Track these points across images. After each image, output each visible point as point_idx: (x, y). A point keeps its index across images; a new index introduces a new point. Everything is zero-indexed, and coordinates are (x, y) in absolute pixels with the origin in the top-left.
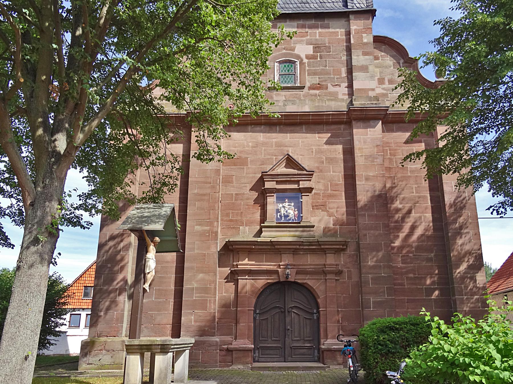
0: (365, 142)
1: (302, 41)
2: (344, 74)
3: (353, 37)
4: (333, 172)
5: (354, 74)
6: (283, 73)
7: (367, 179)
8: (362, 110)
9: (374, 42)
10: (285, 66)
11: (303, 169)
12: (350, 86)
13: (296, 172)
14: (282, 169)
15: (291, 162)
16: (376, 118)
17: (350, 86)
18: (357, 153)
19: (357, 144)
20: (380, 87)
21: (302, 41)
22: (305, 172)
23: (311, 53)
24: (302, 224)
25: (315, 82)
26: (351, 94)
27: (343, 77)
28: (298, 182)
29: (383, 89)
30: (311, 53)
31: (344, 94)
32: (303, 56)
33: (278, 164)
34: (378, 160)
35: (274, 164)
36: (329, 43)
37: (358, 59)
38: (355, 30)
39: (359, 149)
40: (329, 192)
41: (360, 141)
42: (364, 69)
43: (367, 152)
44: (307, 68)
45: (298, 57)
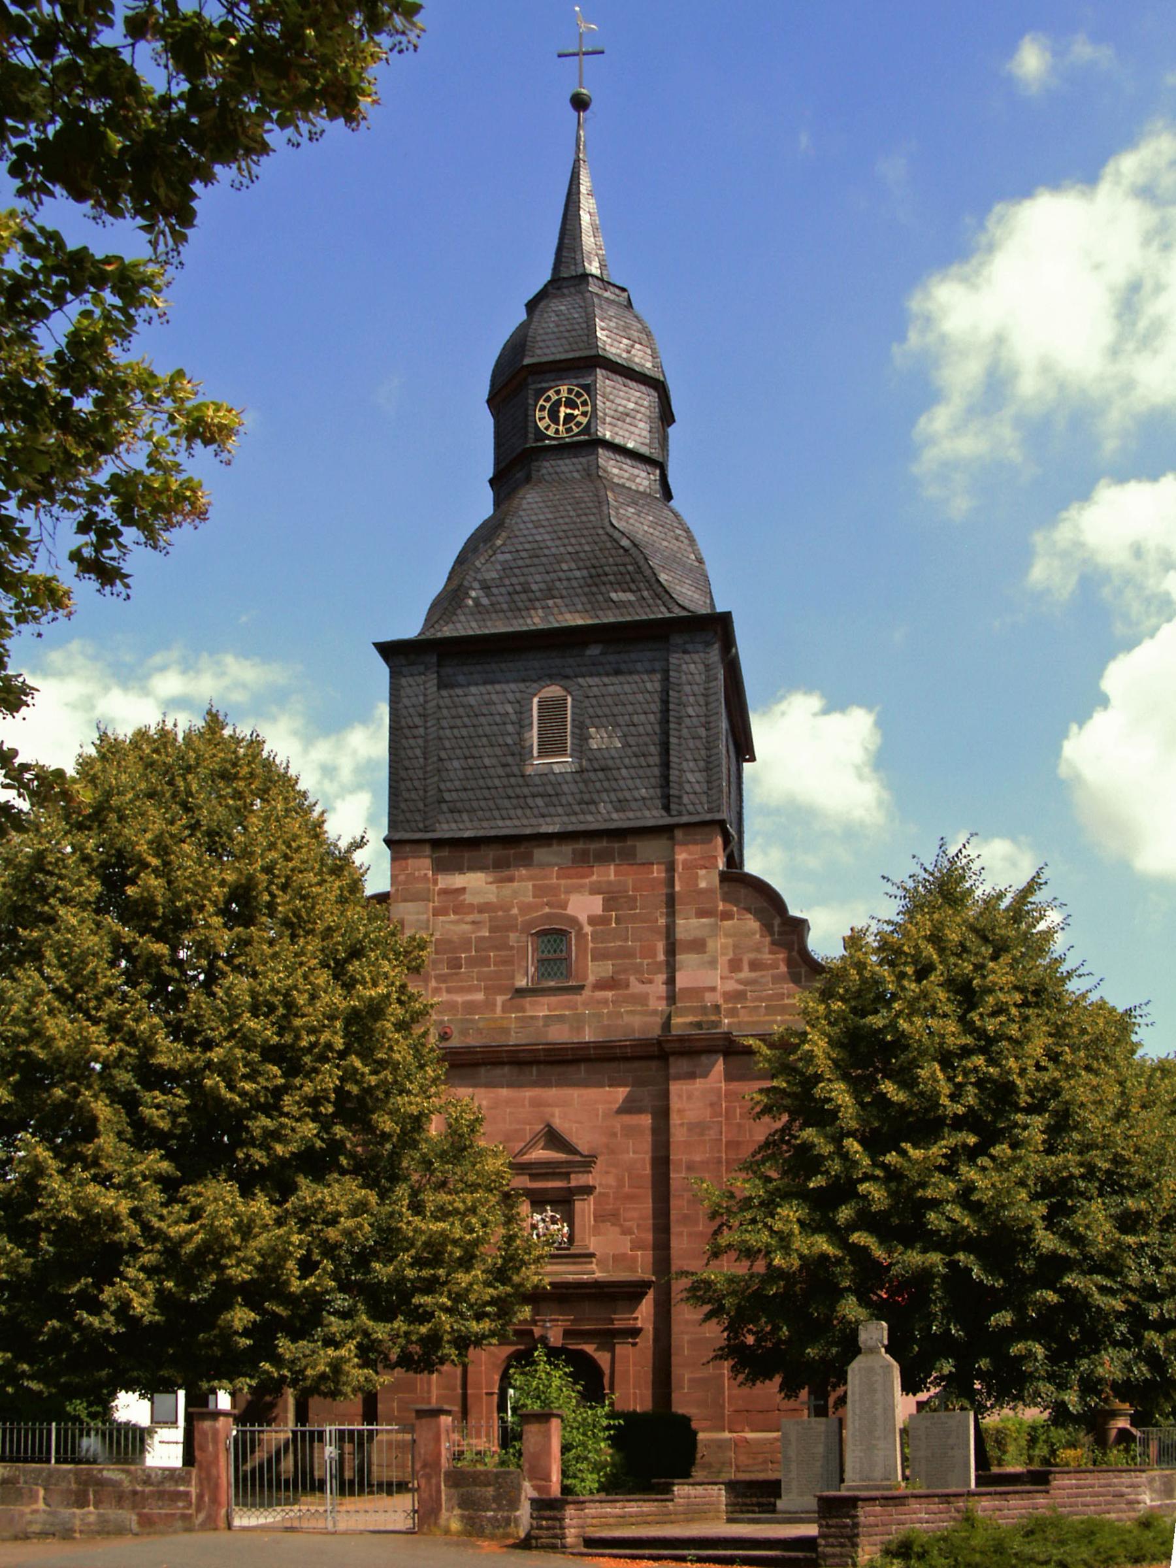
0: (690, 1097)
1: (582, 886)
2: (661, 957)
3: (680, 878)
4: (634, 1152)
5: (678, 957)
6: (545, 955)
7: (690, 1167)
8: (681, 1039)
9: (721, 881)
10: (549, 941)
11: (574, 1152)
12: (671, 981)
13: (561, 1156)
14: (540, 1154)
15: (553, 1138)
16: (711, 1051)
17: (671, 981)
18: (675, 1120)
19: (675, 1104)
20: (732, 978)
21: (582, 886)
22: (578, 1158)
23: (598, 910)
24: (572, 1251)
25: (603, 974)
26: (671, 998)
27: (660, 962)
28: (567, 1176)
29: (739, 982)
30: (598, 910)
31: (659, 998)
32: (583, 918)
33: (530, 1146)
34: (712, 1132)
35: (528, 1139)
36: (634, 889)
37: (688, 926)
38: (685, 862)
39: (679, 1111)
40: (626, 1189)
41: (680, 1096)
42: (698, 946)
43: (692, 1116)
44: (591, 945)
45: (574, 921)
